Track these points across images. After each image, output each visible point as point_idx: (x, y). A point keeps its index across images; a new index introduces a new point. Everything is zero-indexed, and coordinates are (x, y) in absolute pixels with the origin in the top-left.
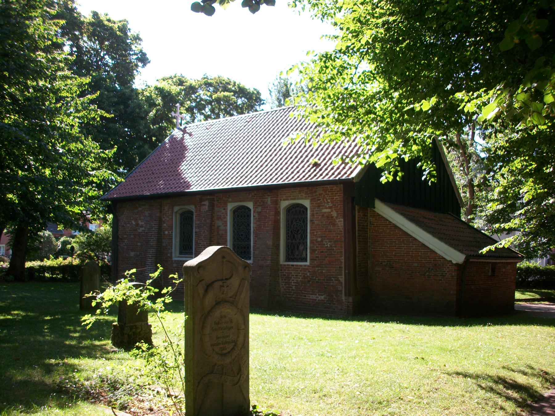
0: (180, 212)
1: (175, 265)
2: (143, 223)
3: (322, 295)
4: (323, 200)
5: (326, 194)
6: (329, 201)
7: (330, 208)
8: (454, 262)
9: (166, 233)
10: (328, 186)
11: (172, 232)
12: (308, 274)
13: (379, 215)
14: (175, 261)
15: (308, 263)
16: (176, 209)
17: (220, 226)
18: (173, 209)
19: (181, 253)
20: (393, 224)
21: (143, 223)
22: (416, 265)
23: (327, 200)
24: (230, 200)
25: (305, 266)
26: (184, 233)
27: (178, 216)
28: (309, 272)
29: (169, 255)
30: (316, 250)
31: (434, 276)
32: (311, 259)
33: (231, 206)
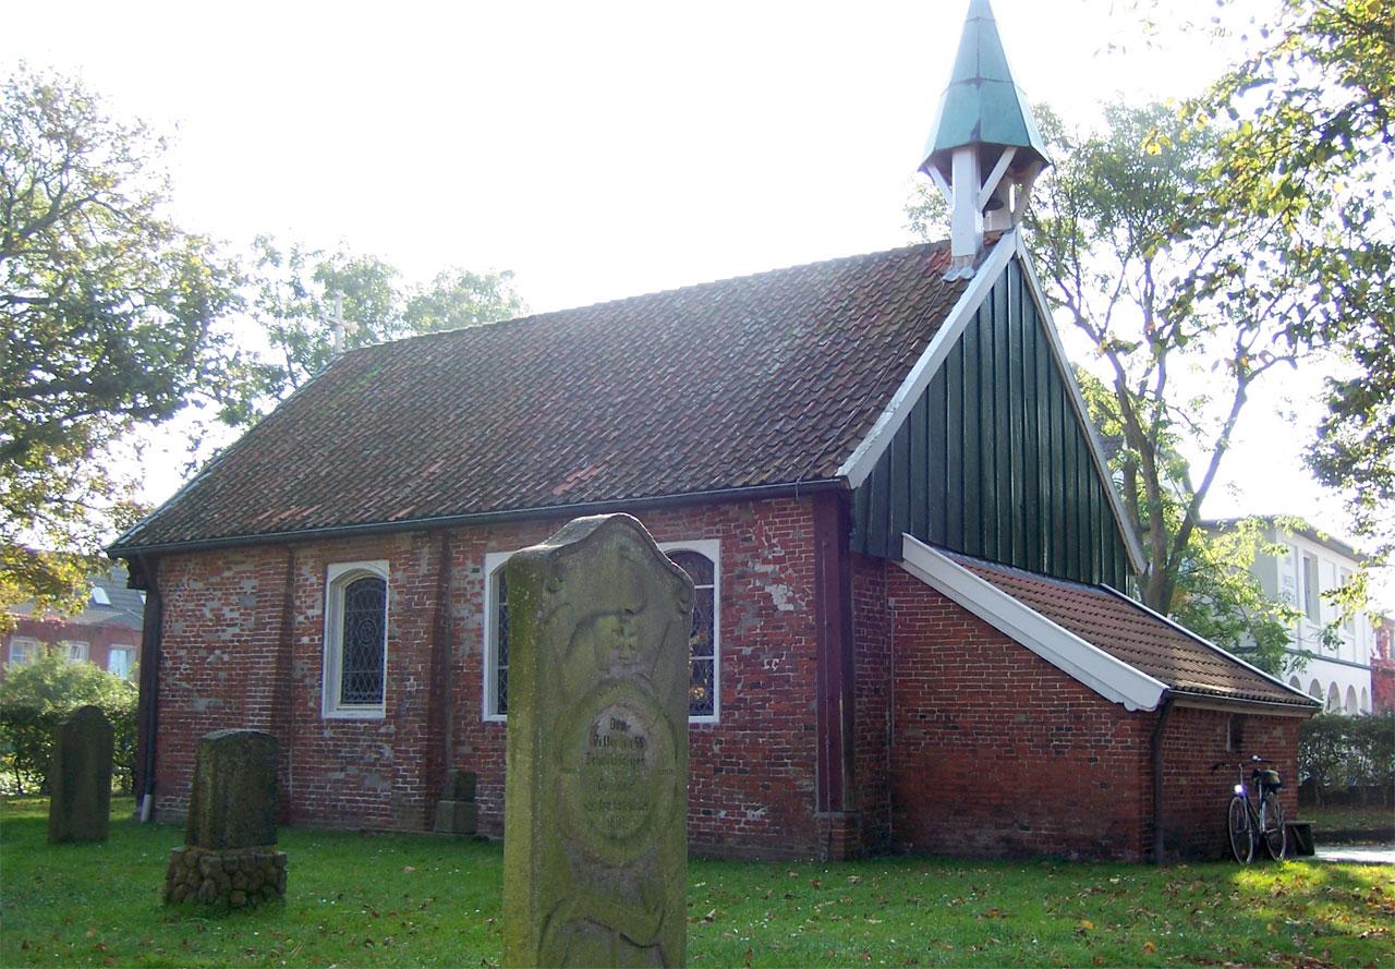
0: (347, 582)
1: (328, 733)
2: (236, 615)
3: (756, 809)
4: (758, 538)
5: (766, 524)
6: (774, 541)
7: (777, 560)
8: (1130, 707)
9: (305, 640)
10: (773, 501)
11: (322, 639)
12: (716, 748)
13: (916, 581)
14: (330, 720)
15: (714, 719)
16: (335, 570)
17: (462, 619)
18: (325, 573)
19: (342, 702)
21: (236, 615)
22: (1022, 718)
23: (768, 539)
24: (493, 544)
25: (707, 726)
26: (355, 642)
27: (341, 595)
28: (721, 742)
29: (311, 704)
30: (739, 681)
32: (723, 708)
33: (495, 560)
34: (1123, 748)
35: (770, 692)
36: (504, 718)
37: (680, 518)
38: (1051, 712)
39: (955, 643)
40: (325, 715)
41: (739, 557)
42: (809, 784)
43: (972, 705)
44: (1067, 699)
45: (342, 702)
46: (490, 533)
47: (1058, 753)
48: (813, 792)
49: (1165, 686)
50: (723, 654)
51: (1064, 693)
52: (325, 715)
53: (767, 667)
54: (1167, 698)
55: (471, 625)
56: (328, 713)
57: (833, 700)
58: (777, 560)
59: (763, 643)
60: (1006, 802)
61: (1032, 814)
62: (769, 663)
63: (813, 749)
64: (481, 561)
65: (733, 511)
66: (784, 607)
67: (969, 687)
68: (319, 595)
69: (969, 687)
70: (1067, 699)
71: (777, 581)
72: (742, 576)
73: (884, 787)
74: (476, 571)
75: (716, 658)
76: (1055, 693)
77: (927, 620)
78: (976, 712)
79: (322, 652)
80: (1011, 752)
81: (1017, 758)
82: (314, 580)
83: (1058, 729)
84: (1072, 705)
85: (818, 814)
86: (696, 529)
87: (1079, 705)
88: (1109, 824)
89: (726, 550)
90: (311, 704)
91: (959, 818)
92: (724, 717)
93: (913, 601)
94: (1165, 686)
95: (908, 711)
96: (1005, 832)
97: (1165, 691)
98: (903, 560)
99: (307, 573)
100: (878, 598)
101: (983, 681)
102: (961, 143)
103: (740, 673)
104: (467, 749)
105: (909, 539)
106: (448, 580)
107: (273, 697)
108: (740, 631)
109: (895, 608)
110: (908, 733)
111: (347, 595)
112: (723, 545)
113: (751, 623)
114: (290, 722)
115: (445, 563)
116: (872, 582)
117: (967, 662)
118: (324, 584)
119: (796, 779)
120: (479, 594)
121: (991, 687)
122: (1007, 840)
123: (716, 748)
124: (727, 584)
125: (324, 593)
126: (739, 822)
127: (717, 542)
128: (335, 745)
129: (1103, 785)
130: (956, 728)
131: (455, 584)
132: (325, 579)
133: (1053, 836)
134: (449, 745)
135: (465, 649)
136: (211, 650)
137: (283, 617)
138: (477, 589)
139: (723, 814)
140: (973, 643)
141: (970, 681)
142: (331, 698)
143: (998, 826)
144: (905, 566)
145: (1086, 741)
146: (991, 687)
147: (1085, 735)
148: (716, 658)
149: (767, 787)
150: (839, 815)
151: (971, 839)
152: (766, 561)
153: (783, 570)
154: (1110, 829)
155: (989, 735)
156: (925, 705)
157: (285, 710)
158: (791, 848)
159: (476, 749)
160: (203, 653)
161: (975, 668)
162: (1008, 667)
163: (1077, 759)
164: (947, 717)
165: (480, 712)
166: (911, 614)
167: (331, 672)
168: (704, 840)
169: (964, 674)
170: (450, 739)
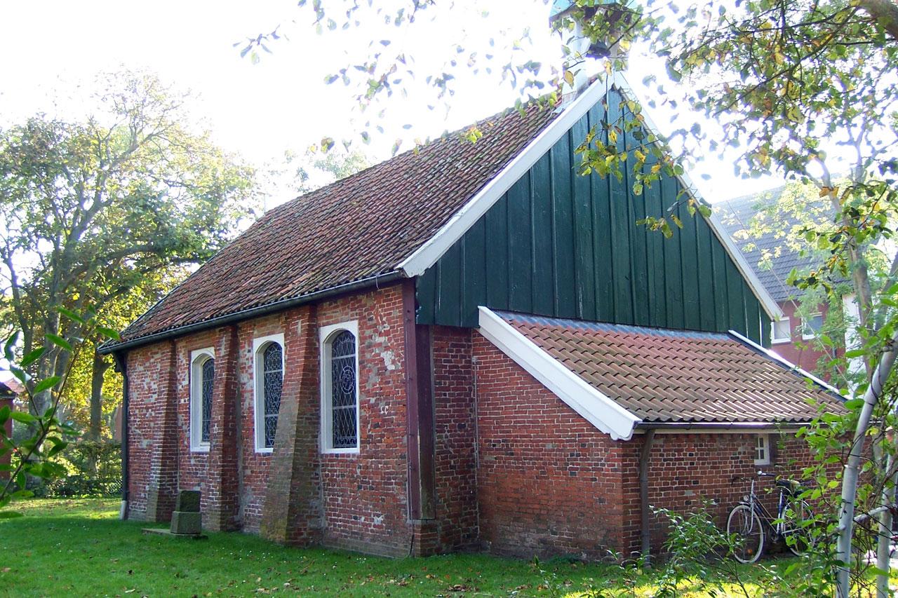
6: (384, 319)
7: (387, 333)
8: (614, 437)
12: (358, 471)
13: (488, 343)
14: (193, 453)
17: (245, 384)
18: (190, 357)
19: (203, 441)
20: (511, 360)
27: (200, 370)
28: (360, 467)
31: (582, 469)
33: (258, 343)
34: (610, 467)
35: (385, 431)
36: (270, 450)
37: (337, 307)
38: (567, 441)
39: (511, 389)
40: (192, 450)
41: (368, 332)
42: (404, 499)
43: (521, 437)
44: (576, 431)
45: (203, 441)
46: (255, 325)
47: (572, 474)
48: (406, 505)
49: (637, 419)
50: (361, 403)
51: (574, 426)
52: (192, 450)
53: (382, 412)
54: (644, 433)
55: (249, 388)
56: (194, 449)
57: (414, 436)
58: (387, 333)
59: (381, 395)
60: (542, 512)
61: (558, 522)
62: (383, 410)
63: (405, 473)
64: (251, 344)
65: (364, 299)
66: (391, 367)
67: (519, 422)
68: (187, 371)
69: (519, 422)
70: (576, 431)
71: (387, 348)
72: (369, 346)
73: (471, 499)
74: (249, 351)
75: (358, 406)
76: (569, 426)
77: (495, 372)
78: (524, 441)
79: (189, 409)
80: (544, 473)
81: (548, 478)
82: (184, 362)
83: (572, 455)
84: (579, 436)
85: (409, 521)
86: (347, 314)
87: (584, 436)
88: (604, 532)
89: (361, 328)
90: (186, 443)
91: (516, 524)
92: (363, 448)
93: (486, 358)
94: (637, 419)
95: (486, 441)
96: (543, 535)
97: (636, 423)
98: (479, 327)
99: (182, 357)
100: (463, 357)
101: (526, 417)
102: (563, 10)
103: (370, 417)
104: (248, 472)
105: (483, 309)
106: (237, 358)
107: (164, 439)
108: (369, 387)
109: (477, 363)
110: (487, 458)
111: (204, 370)
112: (359, 324)
113: (375, 379)
114: (177, 454)
115: (234, 348)
116: (453, 346)
117: (517, 403)
118: (189, 364)
119: (398, 494)
120: (250, 367)
121: (531, 422)
122: (543, 541)
123: (358, 471)
124: (362, 352)
125: (189, 370)
126: (370, 526)
127: (356, 322)
128: (196, 469)
129: (601, 501)
130: (512, 454)
131: (241, 360)
132: (190, 361)
133: (570, 540)
134: (240, 469)
135: (246, 403)
136: (147, 409)
137: (169, 387)
138: (250, 364)
139: (363, 518)
140: (520, 388)
141: (519, 417)
142: (195, 438)
143: (539, 531)
144: (481, 331)
145: (590, 465)
146: (531, 422)
147: (588, 459)
148: (358, 406)
149: (383, 500)
150: (419, 522)
151: (523, 540)
152: (380, 335)
153: (389, 340)
154: (605, 536)
155: (531, 459)
156: (495, 437)
157: (174, 446)
158: (396, 545)
159: (252, 472)
160: (145, 411)
161: (523, 408)
162: (540, 407)
163: (585, 479)
164: (507, 445)
165: (253, 447)
166: (486, 367)
167: (196, 421)
168: (355, 538)
169: (516, 412)
170: (240, 464)
